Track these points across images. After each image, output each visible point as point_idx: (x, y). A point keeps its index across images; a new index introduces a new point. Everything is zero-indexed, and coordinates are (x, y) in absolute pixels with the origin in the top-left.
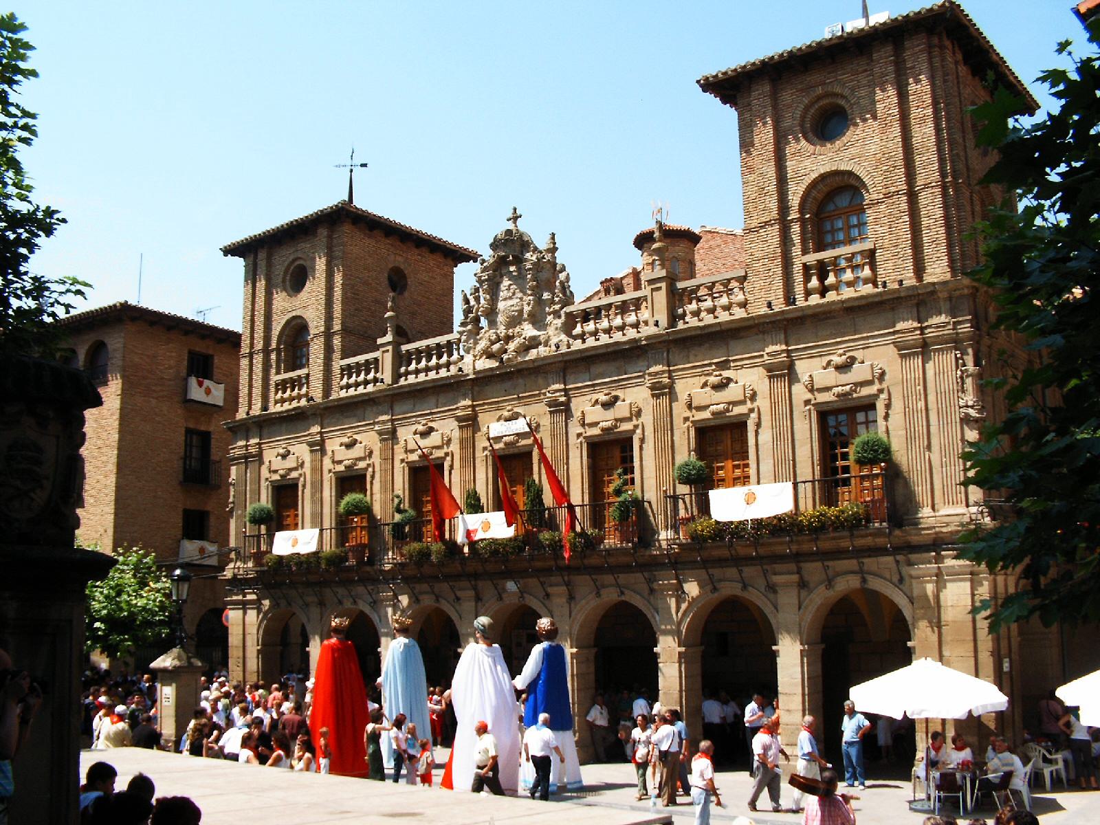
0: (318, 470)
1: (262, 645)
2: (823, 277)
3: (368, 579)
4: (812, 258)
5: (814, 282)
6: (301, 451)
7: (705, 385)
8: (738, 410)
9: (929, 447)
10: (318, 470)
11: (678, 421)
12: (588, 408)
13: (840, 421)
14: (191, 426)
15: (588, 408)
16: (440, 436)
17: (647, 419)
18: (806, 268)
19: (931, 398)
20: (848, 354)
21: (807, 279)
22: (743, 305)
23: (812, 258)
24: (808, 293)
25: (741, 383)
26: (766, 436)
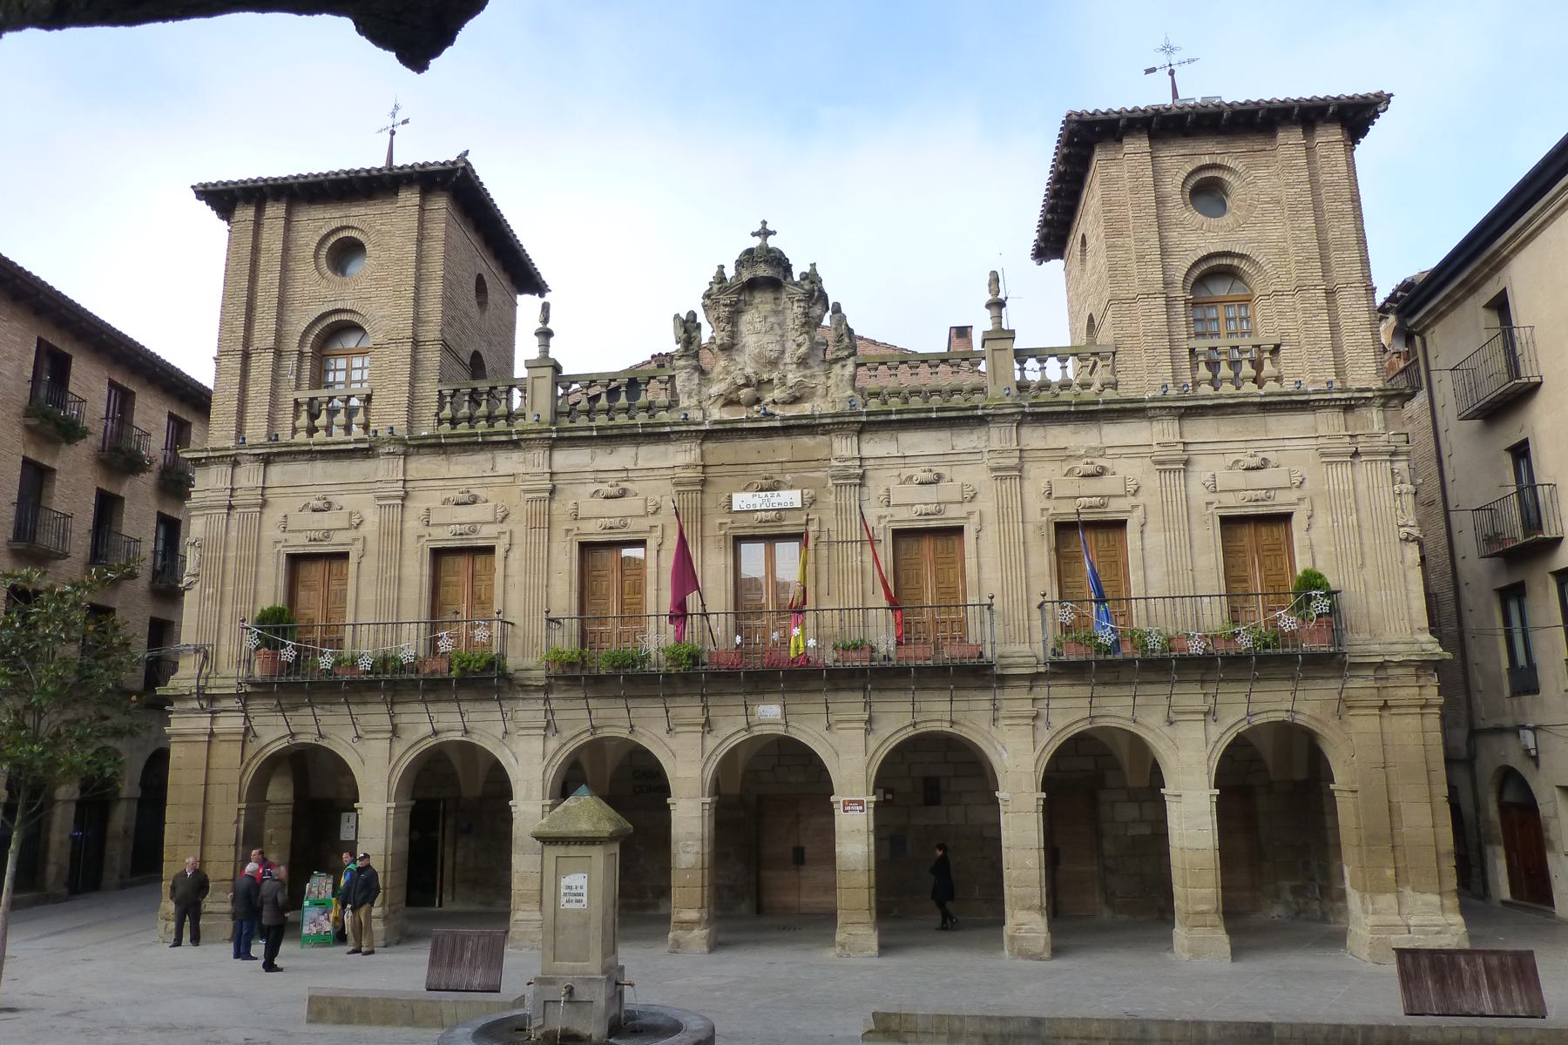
0: (393, 535)
1: (248, 801)
2: (313, 416)
3: (1035, 678)
4: (1201, 345)
5: (304, 420)
6: (976, 476)
7: (1070, 472)
8: (1281, 497)
9: (1363, 565)
10: (393, 535)
11: (409, 539)
12: (894, 485)
13: (1253, 530)
14: (31, 456)
15: (894, 485)
16: (641, 503)
17: (987, 504)
18: (297, 403)
19: (1363, 514)
20: (1262, 455)
21: (296, 416)
22: (1278, 379)
23: (304, 395)
24: (295, 431)
25: (958, 482)
26: (1155, 539)
